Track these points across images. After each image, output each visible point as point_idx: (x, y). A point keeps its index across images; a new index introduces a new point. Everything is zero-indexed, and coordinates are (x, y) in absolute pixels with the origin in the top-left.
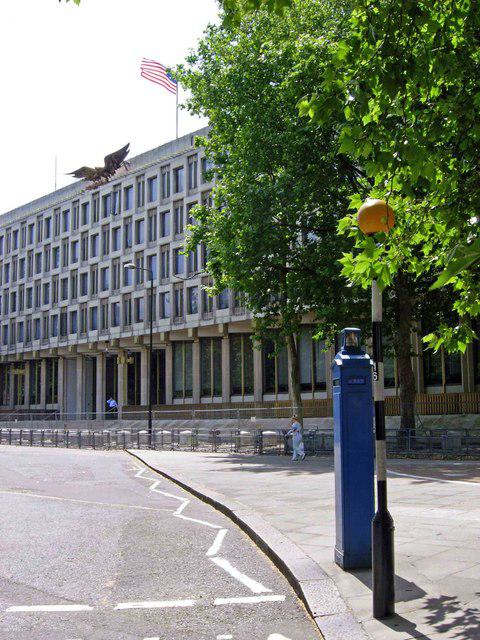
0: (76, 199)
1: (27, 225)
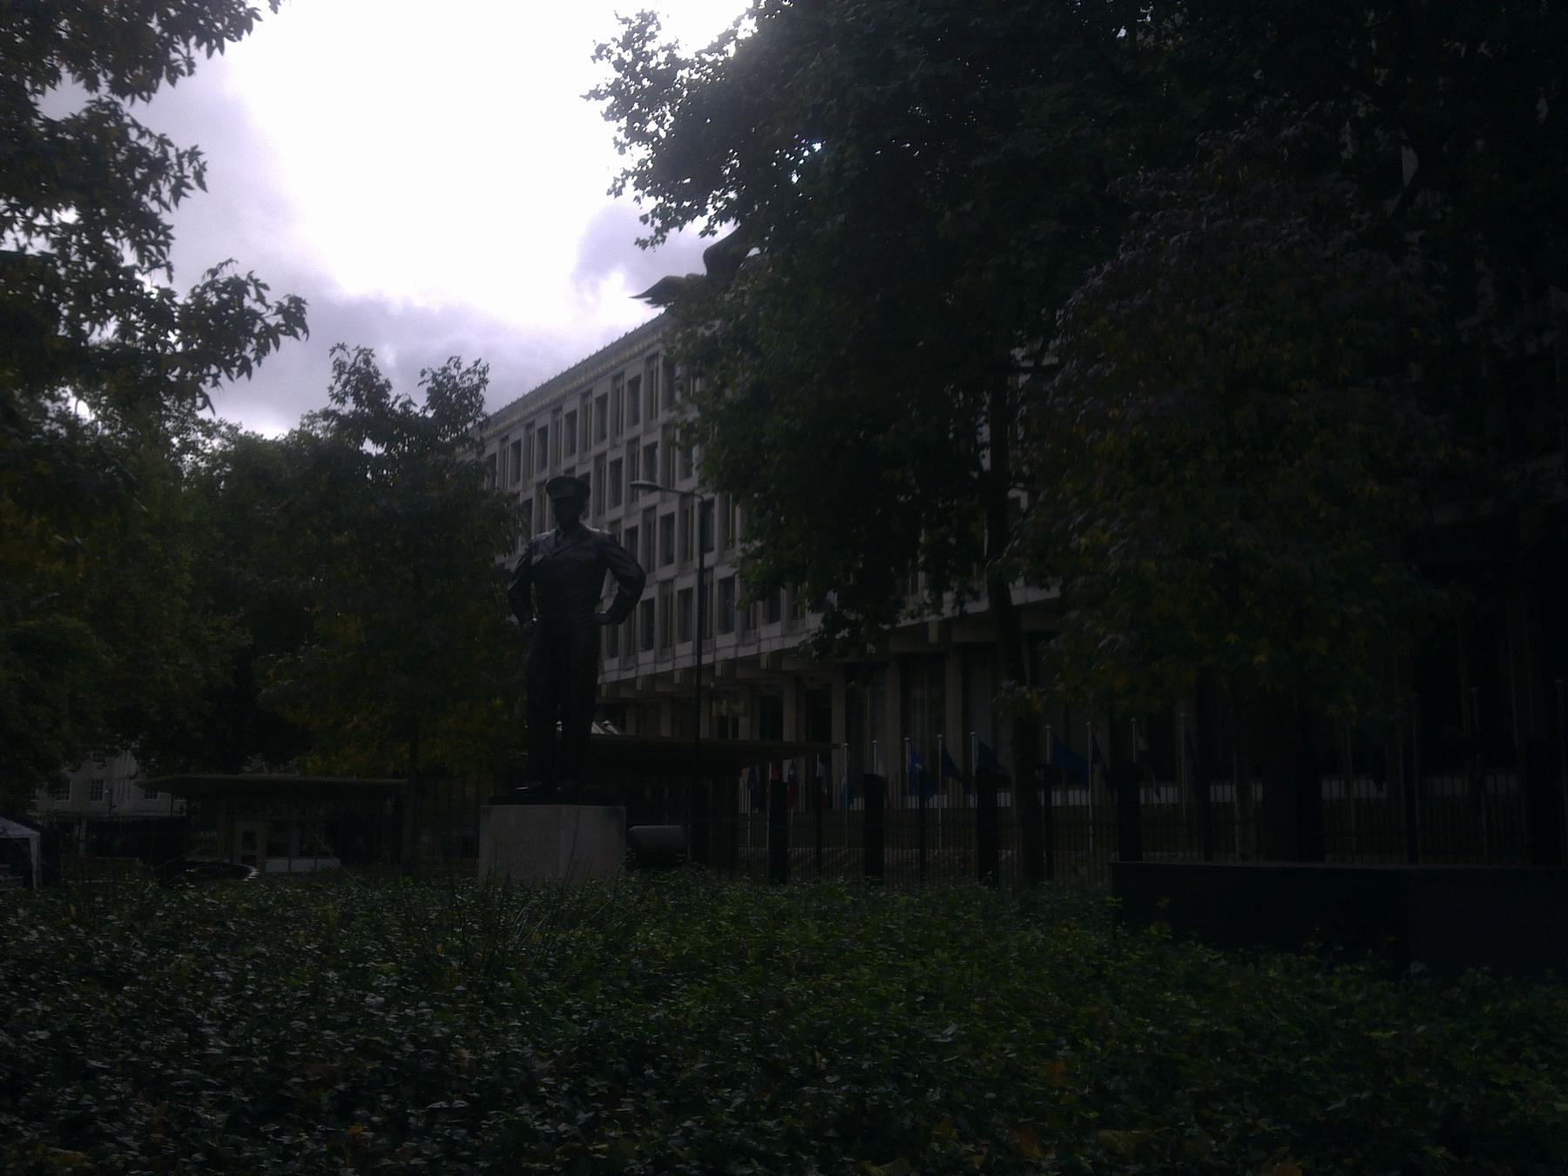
0: (619, 369)
1: (562, 416)
